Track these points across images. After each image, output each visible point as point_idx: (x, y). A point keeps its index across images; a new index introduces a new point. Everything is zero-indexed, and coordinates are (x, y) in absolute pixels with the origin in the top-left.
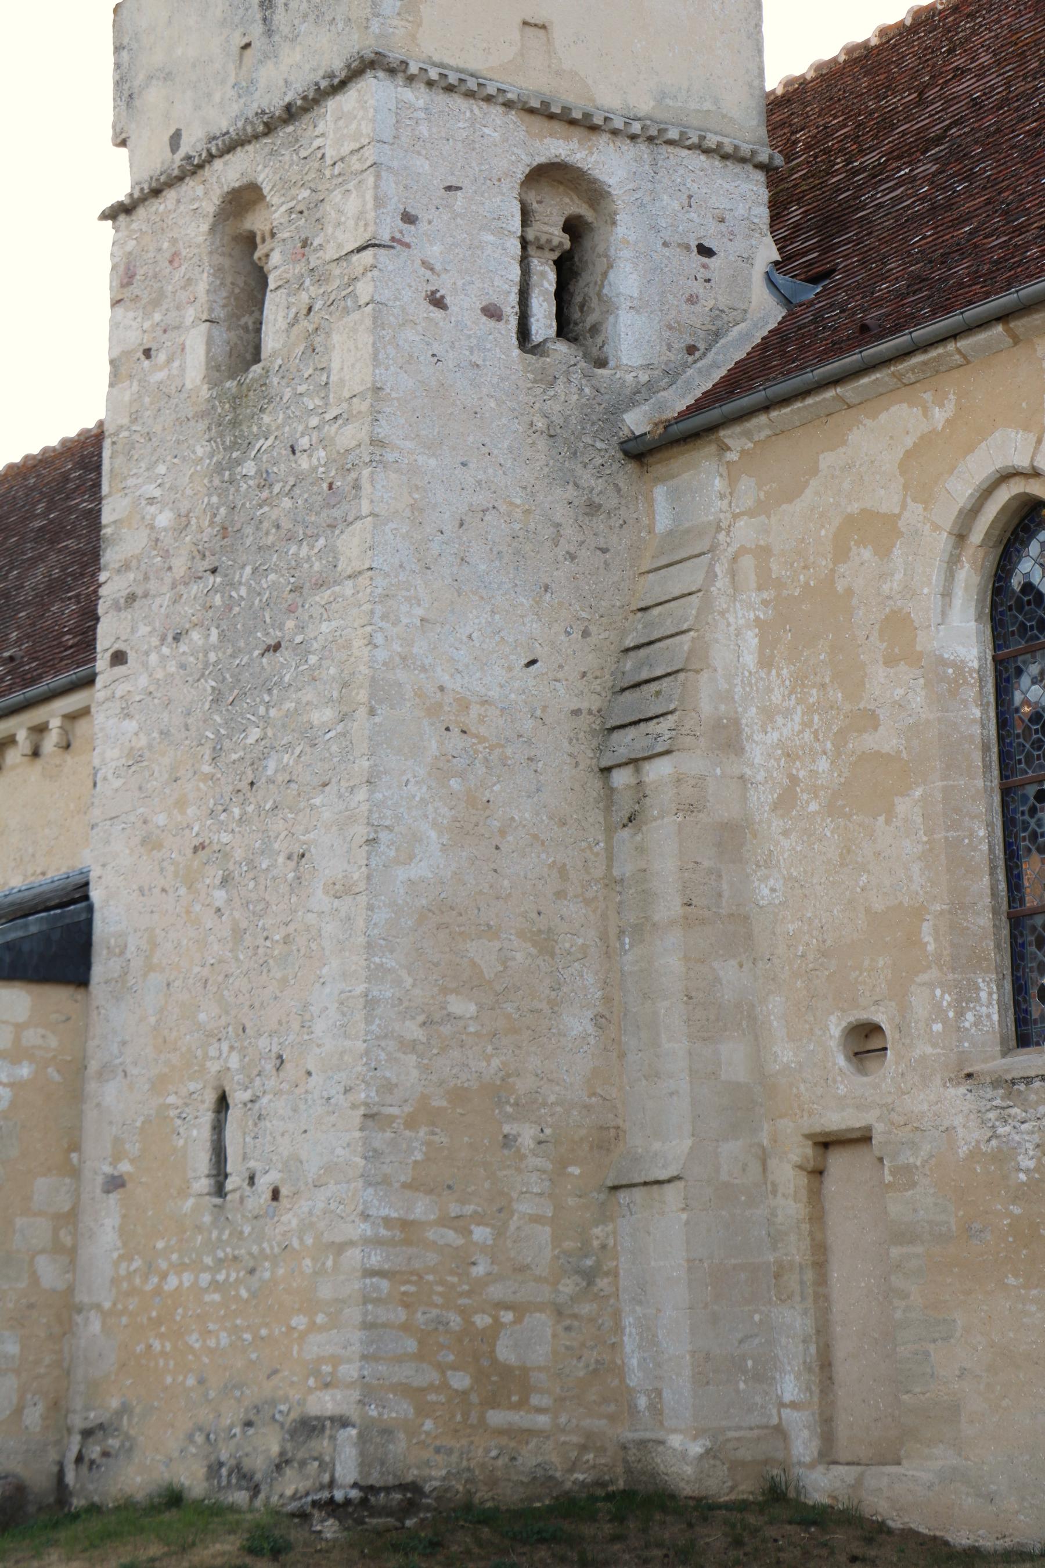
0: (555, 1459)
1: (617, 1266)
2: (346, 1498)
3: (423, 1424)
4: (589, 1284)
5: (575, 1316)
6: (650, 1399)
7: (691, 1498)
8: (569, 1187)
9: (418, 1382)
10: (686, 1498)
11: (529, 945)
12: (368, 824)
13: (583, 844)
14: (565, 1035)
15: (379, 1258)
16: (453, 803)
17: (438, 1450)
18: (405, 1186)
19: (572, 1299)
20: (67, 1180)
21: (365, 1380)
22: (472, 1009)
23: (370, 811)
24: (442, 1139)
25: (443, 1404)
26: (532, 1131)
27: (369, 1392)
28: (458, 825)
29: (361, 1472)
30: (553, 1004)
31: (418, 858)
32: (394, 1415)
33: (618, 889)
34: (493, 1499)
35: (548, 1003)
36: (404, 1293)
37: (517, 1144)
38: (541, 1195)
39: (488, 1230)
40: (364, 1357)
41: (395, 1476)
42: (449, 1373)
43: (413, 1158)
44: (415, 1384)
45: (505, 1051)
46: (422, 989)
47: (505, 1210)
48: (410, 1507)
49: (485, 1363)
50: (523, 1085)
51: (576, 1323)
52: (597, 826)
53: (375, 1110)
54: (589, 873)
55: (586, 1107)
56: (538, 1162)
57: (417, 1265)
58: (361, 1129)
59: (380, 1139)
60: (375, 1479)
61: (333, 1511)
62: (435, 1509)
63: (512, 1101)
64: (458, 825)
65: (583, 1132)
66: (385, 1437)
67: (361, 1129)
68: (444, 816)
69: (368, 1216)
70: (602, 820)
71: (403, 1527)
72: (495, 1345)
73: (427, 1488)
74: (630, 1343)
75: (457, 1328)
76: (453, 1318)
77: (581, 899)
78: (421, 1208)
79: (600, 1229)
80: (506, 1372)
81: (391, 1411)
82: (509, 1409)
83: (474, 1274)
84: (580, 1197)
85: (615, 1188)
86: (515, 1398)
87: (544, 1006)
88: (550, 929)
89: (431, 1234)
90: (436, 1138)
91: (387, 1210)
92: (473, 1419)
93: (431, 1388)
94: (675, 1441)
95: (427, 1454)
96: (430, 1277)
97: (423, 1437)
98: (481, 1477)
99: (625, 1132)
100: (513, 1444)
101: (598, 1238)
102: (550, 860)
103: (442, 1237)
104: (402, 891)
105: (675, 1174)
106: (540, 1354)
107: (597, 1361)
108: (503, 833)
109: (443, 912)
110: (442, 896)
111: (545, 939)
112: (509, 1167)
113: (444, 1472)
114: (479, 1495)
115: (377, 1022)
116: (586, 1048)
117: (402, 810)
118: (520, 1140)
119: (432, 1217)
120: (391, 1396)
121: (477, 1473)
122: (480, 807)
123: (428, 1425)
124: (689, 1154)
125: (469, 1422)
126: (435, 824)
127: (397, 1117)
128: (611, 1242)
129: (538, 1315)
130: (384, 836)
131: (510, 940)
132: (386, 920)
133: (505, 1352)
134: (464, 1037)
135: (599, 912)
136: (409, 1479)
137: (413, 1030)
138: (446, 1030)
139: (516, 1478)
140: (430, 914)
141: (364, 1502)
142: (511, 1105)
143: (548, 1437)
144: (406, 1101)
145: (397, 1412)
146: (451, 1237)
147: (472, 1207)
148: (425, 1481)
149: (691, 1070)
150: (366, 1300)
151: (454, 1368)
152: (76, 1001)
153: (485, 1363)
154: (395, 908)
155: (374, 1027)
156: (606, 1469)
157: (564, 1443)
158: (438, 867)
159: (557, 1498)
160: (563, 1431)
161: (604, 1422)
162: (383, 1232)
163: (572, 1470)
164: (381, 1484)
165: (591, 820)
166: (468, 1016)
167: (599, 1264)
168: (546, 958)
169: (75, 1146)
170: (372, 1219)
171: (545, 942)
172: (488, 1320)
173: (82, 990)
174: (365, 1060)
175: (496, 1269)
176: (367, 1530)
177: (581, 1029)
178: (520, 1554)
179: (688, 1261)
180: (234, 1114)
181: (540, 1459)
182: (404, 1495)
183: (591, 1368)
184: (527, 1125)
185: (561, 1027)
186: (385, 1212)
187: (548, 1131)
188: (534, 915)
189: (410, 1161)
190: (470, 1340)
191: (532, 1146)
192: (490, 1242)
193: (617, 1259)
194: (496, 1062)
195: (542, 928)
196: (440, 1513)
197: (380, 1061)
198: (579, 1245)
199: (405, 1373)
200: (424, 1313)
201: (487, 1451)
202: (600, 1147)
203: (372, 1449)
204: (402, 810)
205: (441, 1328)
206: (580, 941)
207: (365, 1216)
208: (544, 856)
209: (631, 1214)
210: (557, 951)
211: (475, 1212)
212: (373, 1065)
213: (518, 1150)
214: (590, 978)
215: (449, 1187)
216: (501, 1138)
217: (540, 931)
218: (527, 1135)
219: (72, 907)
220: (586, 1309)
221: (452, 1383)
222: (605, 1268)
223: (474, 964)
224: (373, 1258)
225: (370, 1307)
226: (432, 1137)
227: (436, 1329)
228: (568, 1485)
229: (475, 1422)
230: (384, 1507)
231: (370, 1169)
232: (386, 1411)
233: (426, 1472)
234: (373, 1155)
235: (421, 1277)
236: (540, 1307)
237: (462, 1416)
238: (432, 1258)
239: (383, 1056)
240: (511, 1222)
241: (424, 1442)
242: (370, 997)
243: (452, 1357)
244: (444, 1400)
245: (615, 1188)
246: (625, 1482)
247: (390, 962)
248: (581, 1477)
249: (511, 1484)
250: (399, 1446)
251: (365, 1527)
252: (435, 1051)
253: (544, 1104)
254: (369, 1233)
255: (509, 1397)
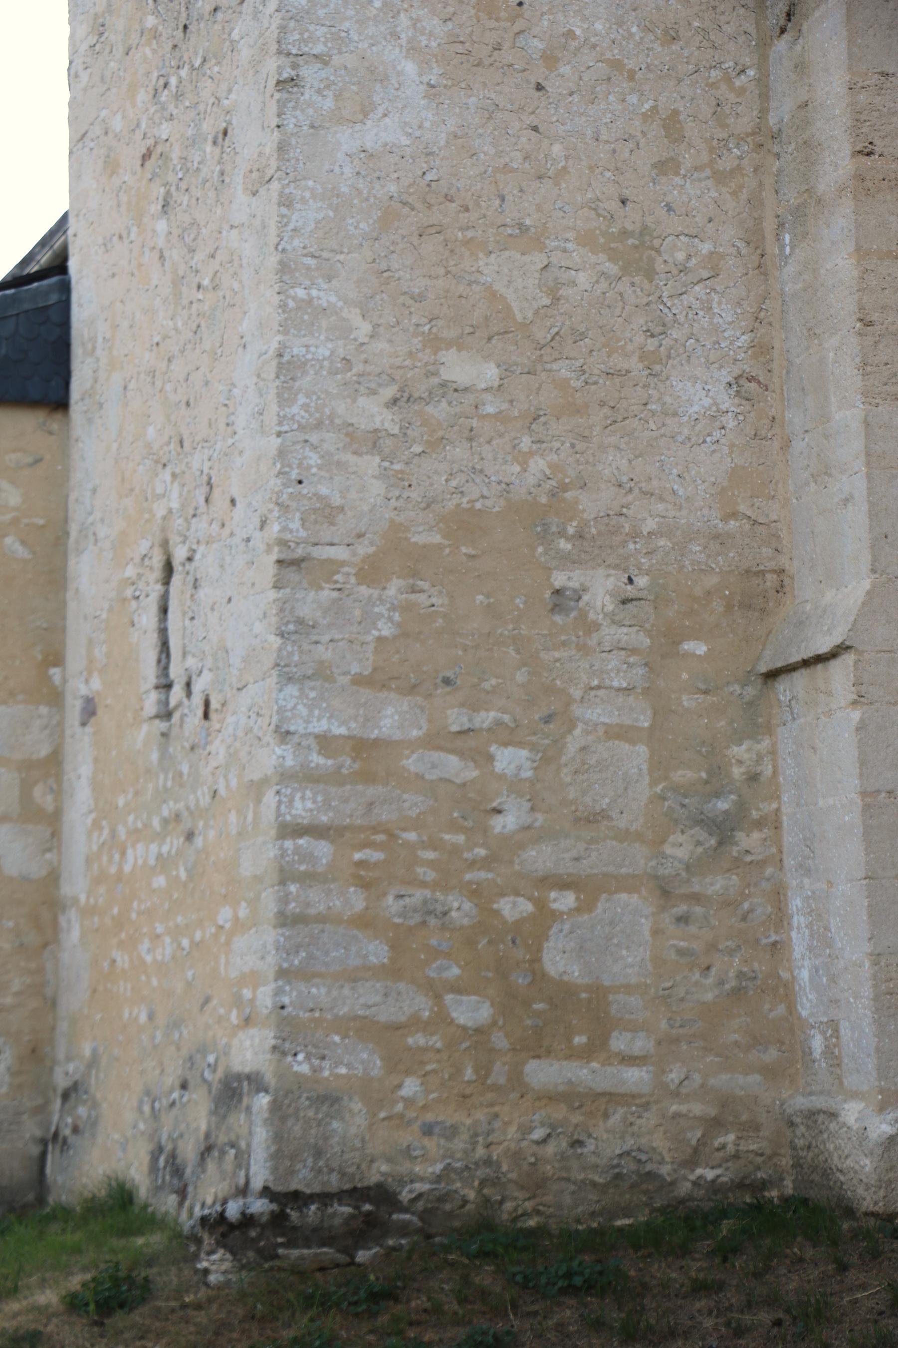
0: (660, 1142)
1: (778, 810)
2: (243, 1214)
3: (399, 1086)
4: (720, 843)
5: (696, 898)
6: (826, 1039)
7: (873, 1214)
8: (685, 676)
9: (387, 1014)
10: (866, 1214)
11: (602, 257)
12: (279, 52)
13: (713, 73)
14: (675, 414)
15: (309, 805)
16: (451, 9)
17: (428, 1130)
18: (359, 681)
19: (688, 867)
20: (44, 710)
21: (285, 1012)
22: (491, 373)
23: (283, 29)
24: (434, 600)
25: (438, 1051)
26: (610, 583)
27: (291, 1033)
28: (460, 48)
29: (275, 1170)
30: (650, 360)
31: (380, 110)
32: (343, 1070)
33: (776, 149)
34: (538, 1212)
35: (641, 359)
36: (362, 864)
37: (581, 604)
38: (628, 690)
39: (524, 753)
40: (282, 974)
41: (343, 1174)
42: (449, 998)
43: (376, 633)
44: (383, 1018)
45: (556, 445)
46: (390, 341)
47: (559, 719)
48: (367, 1228)
49: (521, 980)
50: (591, 504)
51: (698, 910)
52: (742, 39)
53: (300, 552)
54: (724, 126)
55: (716, 537)
56: (623, 635)
57: (385, 814)
58: (277, 586)
59: (311, 603)
60: (303, 1179)
61: (223, 1235)
62: (420, 1231)
63: (571, 531)
64: (460, 48)
65: (711, 581)
66: (325, 1108)
67: (277, 586)
68: (431, 34)
69: (288, 733)
70: (752, 29)
71: (352, 1263)
72: (540, 950)
73: (405, 1196)
74: (799, 942)
75: (466, 921)
76: (456, 905)
77: (708, 172)
78: (392, 718)
79: (744, 747)
80: (562, 995)
81: (337, 1064)
82: (569, 1057)
83: (498, 829)
84: (706, 692)
85: (773, 675)
86: (579, 1040)
87: (634, 364)
88: (645, 230)
89: (412, 763)
90: (422, 598)
91: (324, 722)
92: (499, 1075)
93: (415, 1023)
94: (852, 1113)
95: (407, 1137)
96: (412, 836)
97: (400, 1107)
98: (513, 1176)
99: (792, 578)
100: (577, 1118)
101: (740, 762)
102: (647, 106)
103: (434, 766)
104: (347, 170)
105: (839, 641)
106: (629, 964)
107: (740, 975)
108: (550, 60)
109: (430, 206)
110: (429, 177)
111: (636, 247)
112: (564, 644)
113: (438, 1168)
114: (508, 1206)
115: (302, 399)
116: (717, 434)
117: (346, 25)
118: (586, 598)
119: (415, 733)
120: (337, 1039)
121: (505, 1168)
122: (503, 14)
123: (411, 1087)
124: (863, 604)
125: (489, 1082)
126: (413, 50)
127: (343, 564)
128: (768, 771)
129: (624, 896)
130: (310, 73)
131: (565, 251)
132: (318, 222)
133: (559, 960)
134: (475, 423)
135: (744, 195)
136: (373, 1178)
137: (373, 412)
138: (440, 411)
139: (581, 1177)
140: (406, 210)
141: (278, 1220)
142: (568, 539)
143: (646, 1106)
144: (360, 536)
145: (349, 1066)
146: (453, 766)
147: (492, 714)
148: (402, 1183)
149: (868, 455)
150: (285, 876)
151: (457, 989)
152: (51, 433)
153: (521, 980)
154: (335, 201)
155: (295, 410)
156: (760, 1160)
157: (677, 1115)
158: (420, 127)
159: (662, 1210)
160: (676, 1094)
161: (755, 1078)
162: (316, 759)
163: (692, 1162)
164: (317, 1188)
165: (729, 29)
166: (483, 386)
167: (742, 806)
168: (637, 279)
169: (56, 658)
170: (296, 739)
171: (636, 252)
172: (526, 907)
173: (59, 416)
174: (279, 466)
175: (540, 819)
176: (280, 1269)
177: (707, 402)
178: (529, 1314)
179: (864, 794)
180: (176, 580)
181: (630, 1143)
182: (357, 1208)
183: (727, 987)
184: (601, 571)
185: (668, 399)
186: (321, 726)
187: (642, 581)
188: (614, 205)
189: (369, 638)
190: (490, 942)
191: (610, 608)
192: (529, 774)
193: (779, 797)
194: (538, 465)
195: (630, 227)
196: (429, 1237)
197: (310, 467)
198: (704, 775)
199: (366, 998)
200: (400, 897)
201: (526, 1130)
202: (746, 606)
203: (297, 1129)
204: (346, 25)
205: (433, 921)
206: (706, 248)
207: (284, 735)
208: (633, 99)
209: (794, 719)
210: (660, 266)
211: (499, 723)
212: (294, 475)
213: (583, 615)
214: (725, 313)
215: (447, 681)
216: (548, 594)
217: (625, 233)
218: (600, 589)
219: (35, 284)
220: (717, 884)
221: (454, 1015)
222: (755, 815)
223: (493, 295)
224: (298, 804)
225: (293, 888)
226: (413, 597)
227: (424, 923)
228: (684, 1188)
229: (502, 1081)
230: (316, 1230)
231: (291, 654)
232: (326, 1064)
233: (404, 1167)
234: (295, 629)
235: (392, 836)
236: (628, 883)
237: (476, 1071)
238: (414, 803)
239: (314, 459)
240: (569, 738)
241: (401, 1116)
242: (286, 358)
243: (455, 971)
244: (439, 1045)
245: (773, 675)
246: (794, 1181)
247: (325, 296)
248: (710, 1174)
249: (572, 1187)
250: (353, 1123)
251: (277, 1263)
252: (417, 449)
253: (635, 535)
254: (289, 762)
255: (569, 1040)
